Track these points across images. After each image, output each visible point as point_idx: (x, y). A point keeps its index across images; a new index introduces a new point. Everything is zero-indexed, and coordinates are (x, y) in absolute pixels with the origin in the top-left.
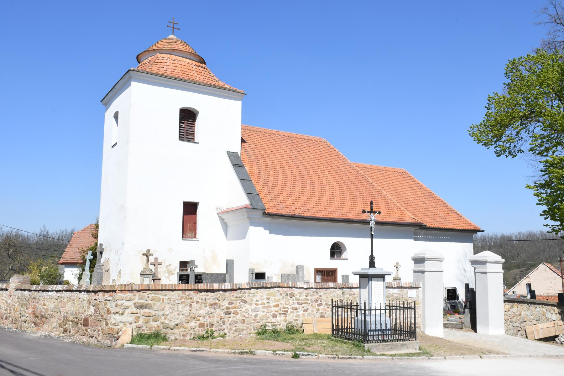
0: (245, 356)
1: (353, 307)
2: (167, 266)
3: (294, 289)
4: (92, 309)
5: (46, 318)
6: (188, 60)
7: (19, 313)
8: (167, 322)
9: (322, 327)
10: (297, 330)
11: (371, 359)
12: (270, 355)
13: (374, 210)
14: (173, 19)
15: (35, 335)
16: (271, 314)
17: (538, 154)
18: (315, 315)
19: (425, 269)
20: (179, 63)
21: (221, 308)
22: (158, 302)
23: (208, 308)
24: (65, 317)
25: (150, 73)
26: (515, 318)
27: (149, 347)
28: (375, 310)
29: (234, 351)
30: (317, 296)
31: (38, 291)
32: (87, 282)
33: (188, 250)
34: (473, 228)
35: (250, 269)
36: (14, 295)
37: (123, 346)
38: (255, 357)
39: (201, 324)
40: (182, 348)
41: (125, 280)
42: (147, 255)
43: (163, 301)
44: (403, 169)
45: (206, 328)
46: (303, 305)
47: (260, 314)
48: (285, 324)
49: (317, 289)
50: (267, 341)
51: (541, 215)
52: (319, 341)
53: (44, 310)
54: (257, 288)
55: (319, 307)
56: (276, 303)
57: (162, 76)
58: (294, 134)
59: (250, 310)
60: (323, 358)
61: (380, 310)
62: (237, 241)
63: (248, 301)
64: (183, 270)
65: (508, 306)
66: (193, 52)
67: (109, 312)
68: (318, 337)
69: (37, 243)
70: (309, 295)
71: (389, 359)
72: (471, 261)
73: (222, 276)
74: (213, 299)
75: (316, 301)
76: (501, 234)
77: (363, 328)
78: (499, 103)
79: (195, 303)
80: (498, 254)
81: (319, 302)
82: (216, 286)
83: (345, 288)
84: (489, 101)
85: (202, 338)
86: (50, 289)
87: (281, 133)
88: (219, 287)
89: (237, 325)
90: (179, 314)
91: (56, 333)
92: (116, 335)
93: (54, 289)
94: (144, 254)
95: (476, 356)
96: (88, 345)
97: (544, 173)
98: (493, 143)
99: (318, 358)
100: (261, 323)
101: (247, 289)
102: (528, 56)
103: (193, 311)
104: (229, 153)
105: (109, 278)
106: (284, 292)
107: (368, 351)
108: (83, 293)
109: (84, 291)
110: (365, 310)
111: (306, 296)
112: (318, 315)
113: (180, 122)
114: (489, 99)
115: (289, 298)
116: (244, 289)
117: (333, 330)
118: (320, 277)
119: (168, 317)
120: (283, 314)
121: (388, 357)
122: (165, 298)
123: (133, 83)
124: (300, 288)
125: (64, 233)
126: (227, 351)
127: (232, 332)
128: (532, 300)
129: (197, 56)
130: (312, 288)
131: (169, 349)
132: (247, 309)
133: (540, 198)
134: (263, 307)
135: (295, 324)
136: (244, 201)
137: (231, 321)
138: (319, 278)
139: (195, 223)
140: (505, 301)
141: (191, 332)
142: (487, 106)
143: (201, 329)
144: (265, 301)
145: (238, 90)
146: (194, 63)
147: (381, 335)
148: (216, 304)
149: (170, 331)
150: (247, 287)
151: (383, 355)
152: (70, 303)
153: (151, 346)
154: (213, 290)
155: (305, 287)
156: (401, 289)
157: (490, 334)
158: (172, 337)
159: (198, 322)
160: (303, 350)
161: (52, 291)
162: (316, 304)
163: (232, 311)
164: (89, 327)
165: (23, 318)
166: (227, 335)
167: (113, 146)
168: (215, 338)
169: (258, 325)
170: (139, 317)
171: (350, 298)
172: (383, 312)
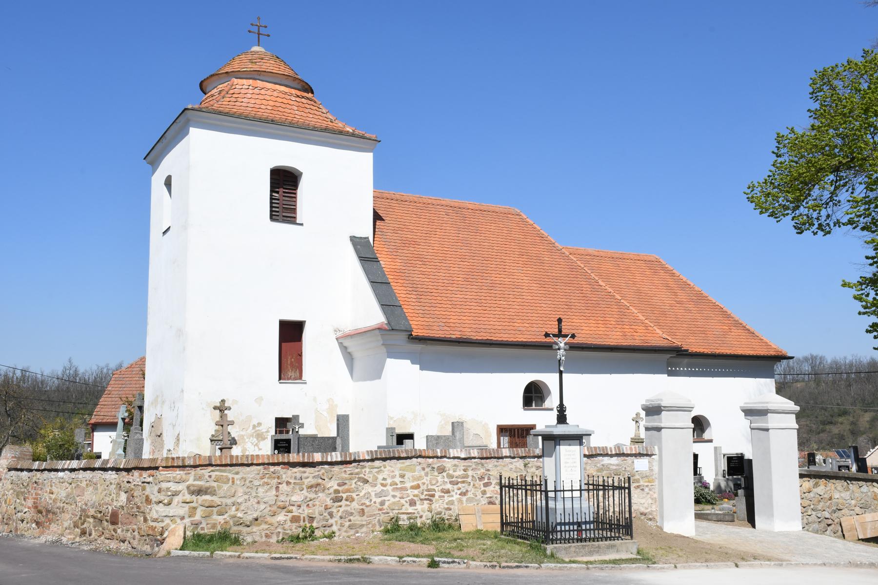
0: (356, 565)
1: (531, 487)
2: (254, 427)
4: (123, 497)
5: (54, 513)
6: (283, 88)
7: (13, 507)
8: (240, 515)
9: (491, 520)
10: (450, 526)
11: (552, 569)
12: (394, 563)
13: (564, 332)
14: (259, 18)
15: (37, 541)
17: (863, 229)
18: (479, 500)
19: (662, 425)
20: (269, 92)
21: (326, 491)
22: (225, 483)
23: (304, 492)
24: (83, 510)
25: (220, 113)
26: (822, 504)
27: (208, 553)
28: (564, 491)
29: (339, 557)
30: (483, 470)
31: (42, 471)
32: (119, 455)
33: (288, 400)
34: (773, 353)
35: (387, 429)
36: (5, 479)
37: (169, 553)
38: (370, 566)
39: (293, 517)
40: (260, 555)
41: (186, 450)
42: (222, 408)
43: (233, 482)
44: (654, 256)
45: (302, 523)
46: (460, 485)
47: (390, 500)
48: (430, 515)
49: (482, 458)
50: (397, 543)
51: (867, 331)
52: (480, 542)
53: (51, 501)
54: (384, 459)
55: (486, 489)
56: (415, 483)
57: (240, 116)
58: (467, 203)
59: (373, 494)
60: (477, 567)
61: (572, 491)
62: (368, 383)
63: (370, 480)
64: (281, 432)
65: (808, 484)
66: (291, 73)
67: (148, 500)
68: (480, 535)
69: (58, 389)
70: (470, 469)
71: (581, 568)
72: (743, 411)
73: (330, 441)
74: (314, 477)
75: (481, 478)
76: (868, 358)
77: (544, 520)
78: (797, 144)
79: (284, 485)
80: (789, 399)
81: (486, 481)
82: (318, 457)
83: (530, 457)
84: (778, 142)
85: (296, 539)
86: (60, 467)
87: (444, 203)
88: (322, 458)
89: (351, 518)
90: (258, 503)
91: (70, 537)
92: (159, 537)
93: (66, 467)
94: (215, 408)
95: (729, 563)
96: (116, 553)
97: (871, 261)
98: (790, 212)
99: (469, 568)
100: (391, 515)
101: (368, 461)
102: (849, 62)
103: (282, 498)
104: (353, 239)
105: (162, 447)
106: (429, 465)
107: (552, 556)
108: (110, 472)
109: (112, 469)
110: (546, 492)
111: (465, 470)
112: (484, 501)
113: (272, 191)
114: (779, 139)
115: (436, 474)
116: (364, 461)
117: (502, 524)
118: (506, 439)
119: (242, 508)
121: (580, 565)
122: (236, 477)
123: (192, 130)
124: (454, 458)
125: (105, 371)
126: (328, 557)
127: (344, 529)
128: (861, 475)
130: (475, 458)
131: (239, 557)
132: (369, 493)
133: (864, 303)
134: (394, 490)
135: (446, 517)
136: (378, 317)
137: (343, 512)
138: (505, 440)
139: (301, 355)
140: (801, 476)
141: (279, 530)
142: (776, 151)
143: (294, 525)
144: (398, 480)
145: (367, 135)
146: (294, 91)
147: (577, 530)
148: (318, 485)
149: (245, 530)
150: (367, 458)
151: (574, 562)
152: (91, 489)
153: (212, 553)
154: (312, 463)
155: (463, 456)
156: (622, 458)
157: (776, 530)
158: (249, 539)
159: (290, 515)
160: (448, 555)
161: (63, 470)
162: (482, 483)
163: (344, 496)
164: (120, 526)
165: (20, 514)
166: (337, 534)
167: (164, 233)
168: (316, 539)
169: (386, 518)
170: (195, 508)
171: (538, 473)
172: (577, 494)
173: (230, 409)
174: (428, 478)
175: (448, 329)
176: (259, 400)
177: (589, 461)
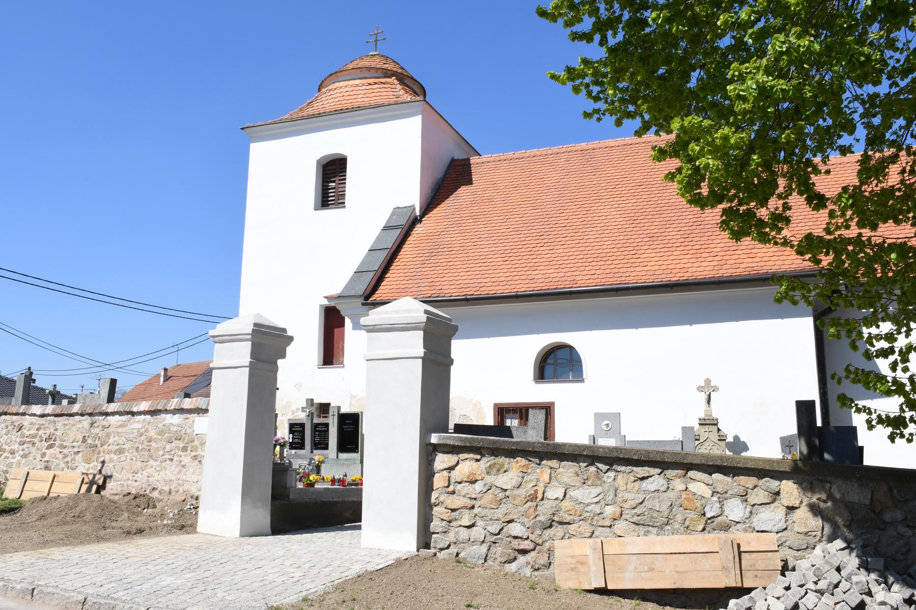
129: (380, 71)
156: (185, 416)
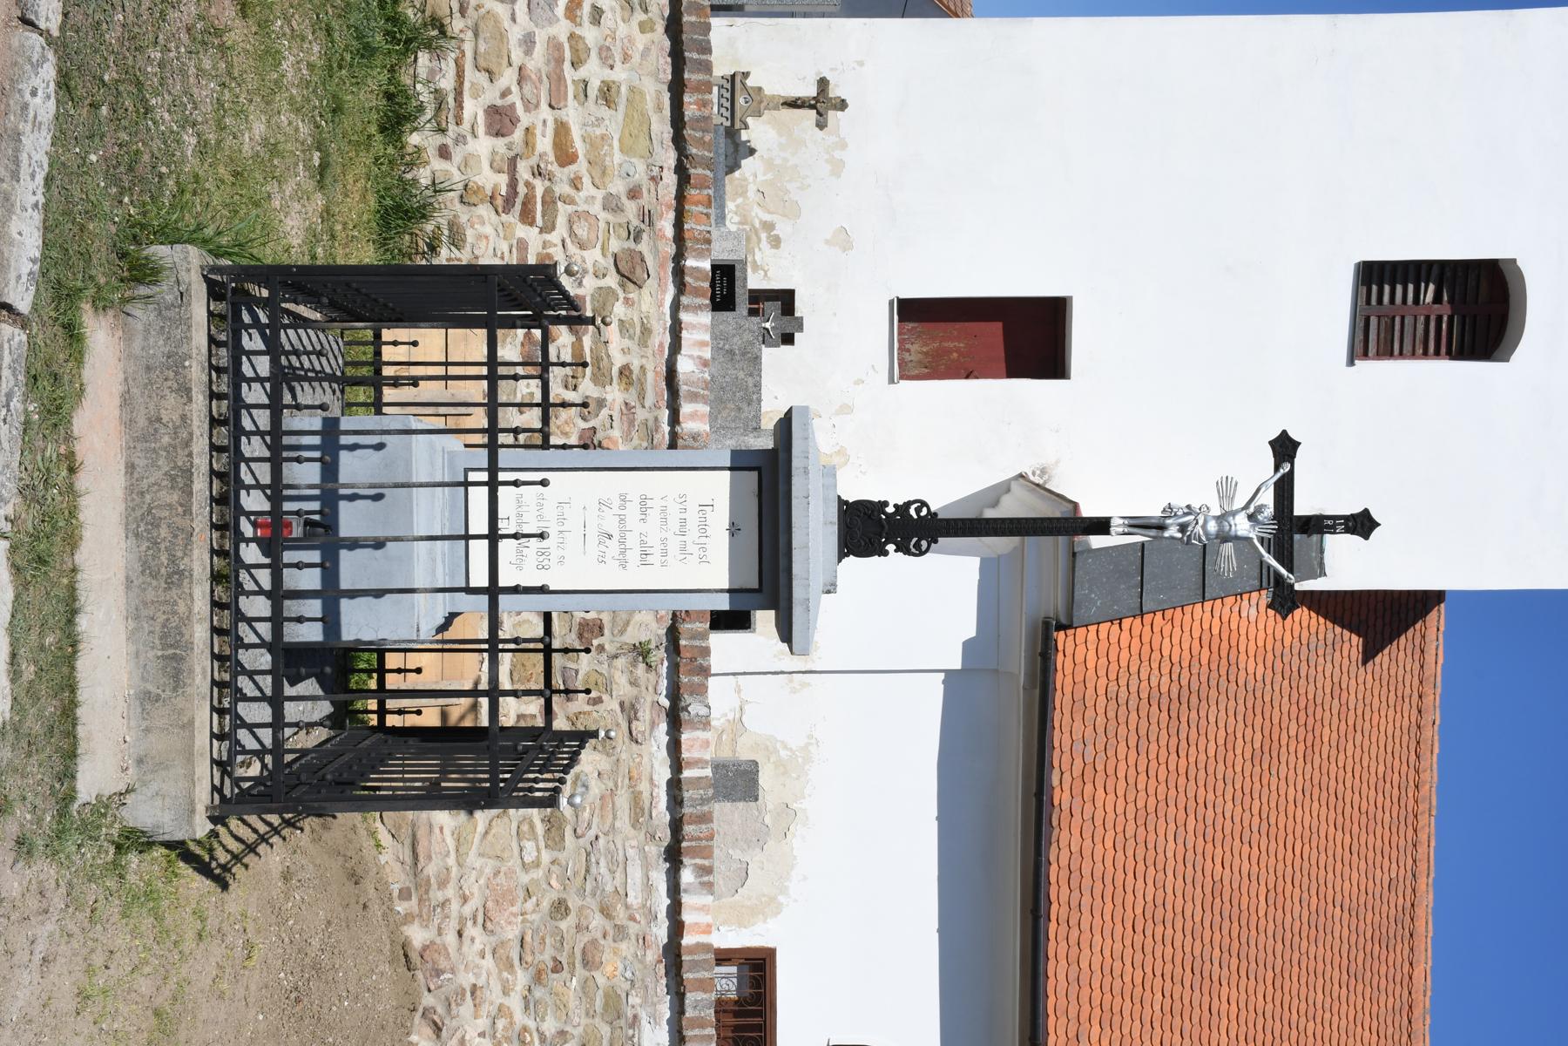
2: (769, 226)
3: (671, 291)
16: (515, 98)
56: (579, 147)
83: (674, 670)
94: (823, 83)
106: (648, 217)
111: (625, 372)
115: (615, 245)
120: (513, 184)
124: (676, 329)
130: (674, 419)
134: (554, 46)
139: (968, 376)
144: (593, 71)
155: (684, 366)
173: (821, 125)
174: (596, 209)
175: (1077, 773)
176: (843, 240)
177: (653, 954)
